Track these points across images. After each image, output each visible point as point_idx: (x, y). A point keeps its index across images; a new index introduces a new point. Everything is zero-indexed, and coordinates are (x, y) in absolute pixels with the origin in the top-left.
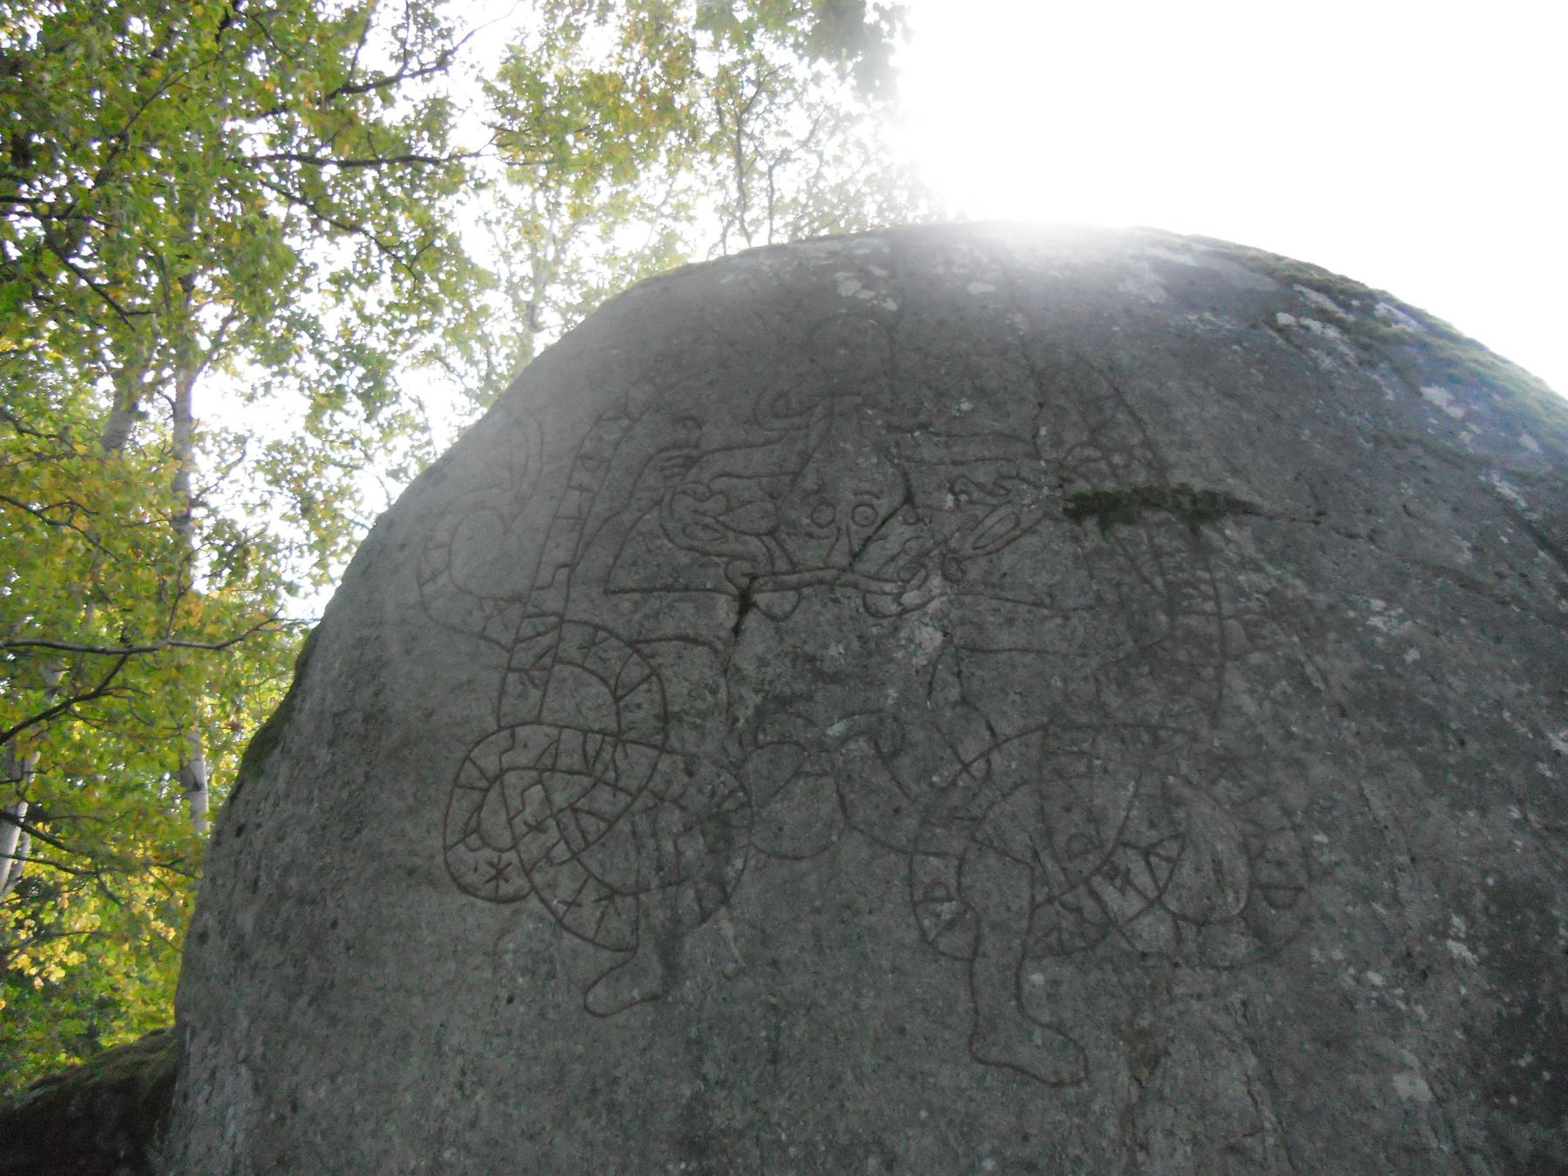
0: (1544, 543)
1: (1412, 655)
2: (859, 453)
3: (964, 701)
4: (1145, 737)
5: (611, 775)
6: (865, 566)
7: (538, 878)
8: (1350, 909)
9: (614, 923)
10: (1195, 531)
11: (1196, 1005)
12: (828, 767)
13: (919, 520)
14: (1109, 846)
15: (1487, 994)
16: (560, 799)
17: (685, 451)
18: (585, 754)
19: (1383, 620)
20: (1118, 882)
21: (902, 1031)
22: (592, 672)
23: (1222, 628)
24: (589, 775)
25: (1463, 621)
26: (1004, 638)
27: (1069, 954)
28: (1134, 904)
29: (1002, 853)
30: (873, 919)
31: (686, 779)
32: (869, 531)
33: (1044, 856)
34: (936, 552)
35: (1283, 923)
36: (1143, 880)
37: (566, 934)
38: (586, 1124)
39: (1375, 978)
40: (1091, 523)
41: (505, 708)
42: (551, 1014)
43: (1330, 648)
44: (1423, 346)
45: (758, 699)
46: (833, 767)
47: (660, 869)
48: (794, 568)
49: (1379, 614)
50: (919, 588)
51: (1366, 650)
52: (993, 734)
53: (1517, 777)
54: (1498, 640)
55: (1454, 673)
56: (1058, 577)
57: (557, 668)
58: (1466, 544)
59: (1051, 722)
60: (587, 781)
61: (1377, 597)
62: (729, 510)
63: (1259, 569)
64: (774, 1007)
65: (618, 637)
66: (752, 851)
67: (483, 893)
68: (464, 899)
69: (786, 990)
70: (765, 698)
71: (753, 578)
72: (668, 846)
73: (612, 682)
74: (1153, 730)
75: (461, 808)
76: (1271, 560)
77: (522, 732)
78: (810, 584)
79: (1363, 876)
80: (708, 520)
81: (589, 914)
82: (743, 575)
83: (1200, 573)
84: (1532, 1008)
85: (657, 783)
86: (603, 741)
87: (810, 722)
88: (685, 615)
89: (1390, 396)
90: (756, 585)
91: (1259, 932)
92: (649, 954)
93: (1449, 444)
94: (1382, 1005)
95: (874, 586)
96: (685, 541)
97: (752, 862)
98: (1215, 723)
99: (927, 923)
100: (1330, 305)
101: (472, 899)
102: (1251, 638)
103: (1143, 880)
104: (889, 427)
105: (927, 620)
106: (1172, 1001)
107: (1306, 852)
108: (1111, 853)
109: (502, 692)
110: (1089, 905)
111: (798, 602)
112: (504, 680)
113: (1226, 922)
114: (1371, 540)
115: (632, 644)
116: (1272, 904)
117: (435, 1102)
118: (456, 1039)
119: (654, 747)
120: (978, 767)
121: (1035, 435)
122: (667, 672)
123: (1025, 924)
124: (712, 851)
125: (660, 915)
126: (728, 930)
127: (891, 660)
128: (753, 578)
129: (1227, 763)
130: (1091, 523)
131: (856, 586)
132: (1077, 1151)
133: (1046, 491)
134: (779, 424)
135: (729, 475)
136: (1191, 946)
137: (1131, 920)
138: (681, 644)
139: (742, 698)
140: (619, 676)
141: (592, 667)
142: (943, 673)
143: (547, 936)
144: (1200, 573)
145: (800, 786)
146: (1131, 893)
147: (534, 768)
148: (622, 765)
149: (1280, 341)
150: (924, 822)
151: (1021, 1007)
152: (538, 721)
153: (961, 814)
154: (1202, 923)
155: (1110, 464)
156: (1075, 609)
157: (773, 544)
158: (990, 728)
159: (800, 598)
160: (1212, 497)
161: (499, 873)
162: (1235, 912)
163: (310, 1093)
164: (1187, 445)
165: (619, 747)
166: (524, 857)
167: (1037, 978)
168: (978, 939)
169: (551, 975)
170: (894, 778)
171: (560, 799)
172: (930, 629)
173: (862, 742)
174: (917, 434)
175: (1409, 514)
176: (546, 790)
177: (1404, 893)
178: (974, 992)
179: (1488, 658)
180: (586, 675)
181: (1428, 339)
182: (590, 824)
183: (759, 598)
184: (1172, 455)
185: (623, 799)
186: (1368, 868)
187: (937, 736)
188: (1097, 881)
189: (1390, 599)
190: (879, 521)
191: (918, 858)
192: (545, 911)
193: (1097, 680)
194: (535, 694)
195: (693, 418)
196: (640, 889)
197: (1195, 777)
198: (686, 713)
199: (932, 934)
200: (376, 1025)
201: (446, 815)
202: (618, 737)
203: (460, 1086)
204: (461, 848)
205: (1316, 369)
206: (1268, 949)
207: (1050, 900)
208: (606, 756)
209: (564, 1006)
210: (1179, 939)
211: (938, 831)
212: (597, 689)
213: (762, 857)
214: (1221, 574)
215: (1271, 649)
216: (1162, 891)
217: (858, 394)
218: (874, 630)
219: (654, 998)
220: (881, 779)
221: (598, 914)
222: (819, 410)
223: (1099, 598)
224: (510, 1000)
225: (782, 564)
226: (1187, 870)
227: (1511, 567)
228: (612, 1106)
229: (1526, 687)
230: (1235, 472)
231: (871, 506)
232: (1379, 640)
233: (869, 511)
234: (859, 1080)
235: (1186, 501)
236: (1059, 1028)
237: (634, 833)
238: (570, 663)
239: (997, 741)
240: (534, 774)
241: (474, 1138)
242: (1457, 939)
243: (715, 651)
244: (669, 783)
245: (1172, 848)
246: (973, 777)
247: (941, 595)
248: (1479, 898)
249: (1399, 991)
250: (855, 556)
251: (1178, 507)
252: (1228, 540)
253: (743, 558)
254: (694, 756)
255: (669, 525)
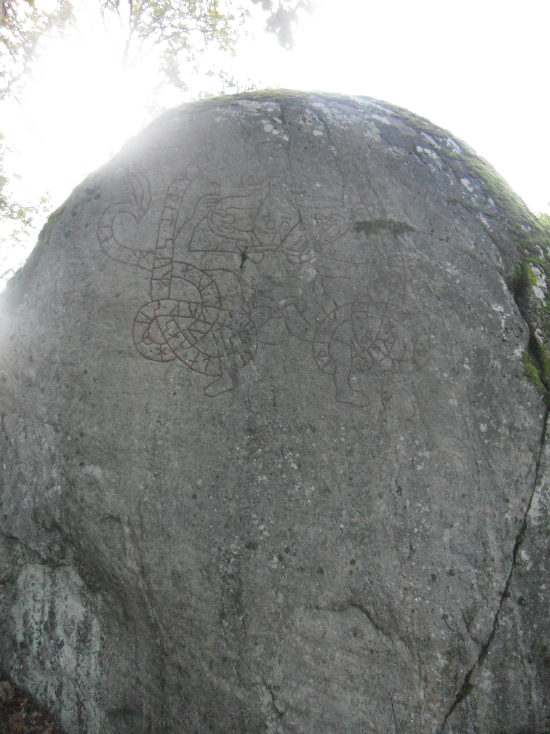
0: (494, 241)
1: (458, 281)
2: (282, 202)
3: (325, 294)
4: (384, 306)
5: (202, 318)
6: (287, 245)
7: (179, 353)
8: (440, 356)
9: (211, 367)
10: (395, 237)
11: (399, 384)
12: (281, 315)
13: (304, 229)
14: (374, 339)
15: (474, 378)
16: (183, 326)
17: (215, 197)
18: (191, 311)
19: (450, 269)
20: (377, 350)
21: (315, 395)
22: (189, 281)
23: (405, 272)
24: (194, 318)
25: (471, 270)
26: (338, 273)
27: (363, 371)
28: (381, 356)
29: (341, 342)
30: (302, 362)
31: (230, 319)
32: (287, 232)
33: (355, 343)
34: (311, 242)
35: (422, 360)
36: (384, 349)
37: (193, 372)
38: (213, 428)
39: (446, 375)
40: (363, 233)
41: (154, 293)
42: (192, 397)
43: (435, 278)
44: (462, 161)
45: (252, 291)
46: (283, 315)
47: (226, 349)
48: (261, 244)
49: (449, 267)
50: (307, 254)
51: (445, 279)
52: (336, 305)
53: (483, 317)
54: (480, 275)
55: (469, 287)
56: (353, 252)
57: (173, 279)
58: (473, 242)
59: (354, 301)
60: (193, 320)
61: (449, 262)
62: (235, 221)
63: (415, 251)
64: (273, 391)
65: (197, 269)
66: (259, 342)
67: (156, 359)
68: (147, 361)
69: (276, 385)
70: (255, 291)
71: (246, 248)
72: (228, 341)
73: (197, 285)
74: (386, 304)
75: (140, 330)
76: (418, 248)
77: (163, 302)
78: (267, 251)
79: (443, 347)
80: (228, 225)
81: (202, 365)
82: (242, 246)
83: (397, 252)
84: (483, 381)
85: (220, 320)
86: (197, 306)
87: (272, 299)
88: (222, 261)
89: (452, 184)
90: (248, 250)
91: (415, 362)
92: (227, 376)
93: (468, 203)
94: (447, 382)
95: (290, 252)
96: (219, 233)
97: (260, 346)
98: (404, 303)
99: (319, 363)
100: (433, 142)
101: (150, 361)
102: (413, 275)
103: (384, 349)
104: (292, 192)
105: (310, 266)
106: (393, 383)
107: (429, 340)
108: (374, 342)
109: (151, 288)
110: (369, 358)
111: (263, 257)
112: (151, 283)
113: (407, 360)
114: (447, 241)
115: (203, 271)
116: (419, 355)
117: (150, 427)
118: (154, 408)
119: (218, 308)
120: (332, 316)
121: (343, 198)
122: (218, 281)
123: (349, 363)
124: (244, 342)
125: (229, 364)
126: (254, 368)
127: (299, 279)
128: (246, 248)
129: (408, 315)
130: (363, 233)
131: (283, 252)
132: (367, 423)
133: (347, 220)
134: (252, 188)
135: (234, 208)
136: (397, 368)
137: (380, 361)
138: (222, 271)
139: (247, 291)
140: (199, 282)
141: (188, 279)
142: (317, 284)
143: (186, 372)
144: (397, 252)
145: (272, 321)
146: (380, 353)
147: (170, 316)
148: (206, 315)
149: (419, 160)
150: (316, 332)
151: (350, 387)
152: (168, 298)
153: (328, 330)
154: (400, 361)
155: (368, 211)
156: (360, 264)
157: (253, 236)
158: (335, 303)
159: (264, 255)
160: (401, 224)
161: (162, 352)
162: (409, 358)
163: (89, 430)
164: (392, 204)
165: (204, 308)
166: (171, 346)
167: (354, 378)
168: (336, 368)
169: (190, 385)
170: (304, 319)
171: (183, 326)
172: (312, 269)
173: (292, 307)
174: (302, 195)
175: (458, 232)
176: (176, 323)
177: (453, 351)
178: (335, 384)
179: (478, 282)
180: (186, 282)
181: (463, 157)
182: (197, 335)
183: (249, 255)
184: (387, 208)
185: (209, 326)
186: (445, 345)
187: (317, 305)
188: (371, 350)
189: (452, 263)
190: (290, 228)
191: (315, 344)
192: (184, 364)
193: (368, 288)
194: (166, 289)
195: (216, 183)
196: (220, 356)
197: (398, 319)
198: (228, 296)
199: (322, 367)
200: (116, 406)
201: (133, 332)
202: (203, 305)
203: (159, 422)
204: (143, 344)
205: (430, 172)
206: (418, 368)
207: (356, 356)
208: (199, 311)
209: (197, 395)
210: (394, 366)
211: (321, 335)
212: (191, 287)
213: (263, 345)
214: (404, 253)
215: (419, 278)
216: (389, 352)
217: (279, 177)
218: (291, 268)
219: (231, 390)
220: (299, 319)
221: (205, 364)
222: (265, 183)
223: (367, 260)
224: (175, 394)
225: (256, 243)
226: (396, 347)
227: (484, 251)
228: (221, 422)
229: (487, 291)
230: (407, 214)
231: (287, 223)
232: (449, 276)
233: (287, 225)
234: (302, 409)
235: (392, 225)
236: (361, 392)
237: (214, 337)
238: (178, 277)
239: (337, 307)
240: (170, 318)
241: (169, 437)
242: (466, 364)
243: (235, 274)
244: (224, 321)
245: (392, 340)
246: (330, 319)
247: (315, 257)
248: (472, 353)
249: (452, 378)
250: (282, 241)
251: (390, 228)
252: (406, 241)
253: (242, 240)
254: (232, 311)
255: (212, 226)
